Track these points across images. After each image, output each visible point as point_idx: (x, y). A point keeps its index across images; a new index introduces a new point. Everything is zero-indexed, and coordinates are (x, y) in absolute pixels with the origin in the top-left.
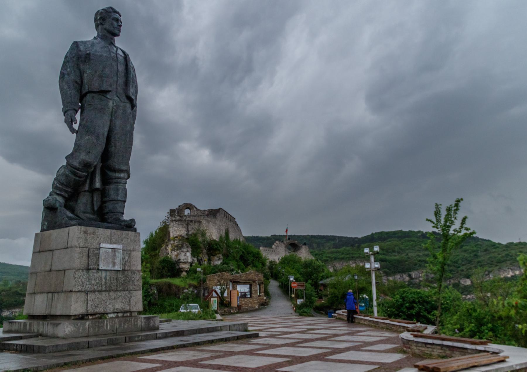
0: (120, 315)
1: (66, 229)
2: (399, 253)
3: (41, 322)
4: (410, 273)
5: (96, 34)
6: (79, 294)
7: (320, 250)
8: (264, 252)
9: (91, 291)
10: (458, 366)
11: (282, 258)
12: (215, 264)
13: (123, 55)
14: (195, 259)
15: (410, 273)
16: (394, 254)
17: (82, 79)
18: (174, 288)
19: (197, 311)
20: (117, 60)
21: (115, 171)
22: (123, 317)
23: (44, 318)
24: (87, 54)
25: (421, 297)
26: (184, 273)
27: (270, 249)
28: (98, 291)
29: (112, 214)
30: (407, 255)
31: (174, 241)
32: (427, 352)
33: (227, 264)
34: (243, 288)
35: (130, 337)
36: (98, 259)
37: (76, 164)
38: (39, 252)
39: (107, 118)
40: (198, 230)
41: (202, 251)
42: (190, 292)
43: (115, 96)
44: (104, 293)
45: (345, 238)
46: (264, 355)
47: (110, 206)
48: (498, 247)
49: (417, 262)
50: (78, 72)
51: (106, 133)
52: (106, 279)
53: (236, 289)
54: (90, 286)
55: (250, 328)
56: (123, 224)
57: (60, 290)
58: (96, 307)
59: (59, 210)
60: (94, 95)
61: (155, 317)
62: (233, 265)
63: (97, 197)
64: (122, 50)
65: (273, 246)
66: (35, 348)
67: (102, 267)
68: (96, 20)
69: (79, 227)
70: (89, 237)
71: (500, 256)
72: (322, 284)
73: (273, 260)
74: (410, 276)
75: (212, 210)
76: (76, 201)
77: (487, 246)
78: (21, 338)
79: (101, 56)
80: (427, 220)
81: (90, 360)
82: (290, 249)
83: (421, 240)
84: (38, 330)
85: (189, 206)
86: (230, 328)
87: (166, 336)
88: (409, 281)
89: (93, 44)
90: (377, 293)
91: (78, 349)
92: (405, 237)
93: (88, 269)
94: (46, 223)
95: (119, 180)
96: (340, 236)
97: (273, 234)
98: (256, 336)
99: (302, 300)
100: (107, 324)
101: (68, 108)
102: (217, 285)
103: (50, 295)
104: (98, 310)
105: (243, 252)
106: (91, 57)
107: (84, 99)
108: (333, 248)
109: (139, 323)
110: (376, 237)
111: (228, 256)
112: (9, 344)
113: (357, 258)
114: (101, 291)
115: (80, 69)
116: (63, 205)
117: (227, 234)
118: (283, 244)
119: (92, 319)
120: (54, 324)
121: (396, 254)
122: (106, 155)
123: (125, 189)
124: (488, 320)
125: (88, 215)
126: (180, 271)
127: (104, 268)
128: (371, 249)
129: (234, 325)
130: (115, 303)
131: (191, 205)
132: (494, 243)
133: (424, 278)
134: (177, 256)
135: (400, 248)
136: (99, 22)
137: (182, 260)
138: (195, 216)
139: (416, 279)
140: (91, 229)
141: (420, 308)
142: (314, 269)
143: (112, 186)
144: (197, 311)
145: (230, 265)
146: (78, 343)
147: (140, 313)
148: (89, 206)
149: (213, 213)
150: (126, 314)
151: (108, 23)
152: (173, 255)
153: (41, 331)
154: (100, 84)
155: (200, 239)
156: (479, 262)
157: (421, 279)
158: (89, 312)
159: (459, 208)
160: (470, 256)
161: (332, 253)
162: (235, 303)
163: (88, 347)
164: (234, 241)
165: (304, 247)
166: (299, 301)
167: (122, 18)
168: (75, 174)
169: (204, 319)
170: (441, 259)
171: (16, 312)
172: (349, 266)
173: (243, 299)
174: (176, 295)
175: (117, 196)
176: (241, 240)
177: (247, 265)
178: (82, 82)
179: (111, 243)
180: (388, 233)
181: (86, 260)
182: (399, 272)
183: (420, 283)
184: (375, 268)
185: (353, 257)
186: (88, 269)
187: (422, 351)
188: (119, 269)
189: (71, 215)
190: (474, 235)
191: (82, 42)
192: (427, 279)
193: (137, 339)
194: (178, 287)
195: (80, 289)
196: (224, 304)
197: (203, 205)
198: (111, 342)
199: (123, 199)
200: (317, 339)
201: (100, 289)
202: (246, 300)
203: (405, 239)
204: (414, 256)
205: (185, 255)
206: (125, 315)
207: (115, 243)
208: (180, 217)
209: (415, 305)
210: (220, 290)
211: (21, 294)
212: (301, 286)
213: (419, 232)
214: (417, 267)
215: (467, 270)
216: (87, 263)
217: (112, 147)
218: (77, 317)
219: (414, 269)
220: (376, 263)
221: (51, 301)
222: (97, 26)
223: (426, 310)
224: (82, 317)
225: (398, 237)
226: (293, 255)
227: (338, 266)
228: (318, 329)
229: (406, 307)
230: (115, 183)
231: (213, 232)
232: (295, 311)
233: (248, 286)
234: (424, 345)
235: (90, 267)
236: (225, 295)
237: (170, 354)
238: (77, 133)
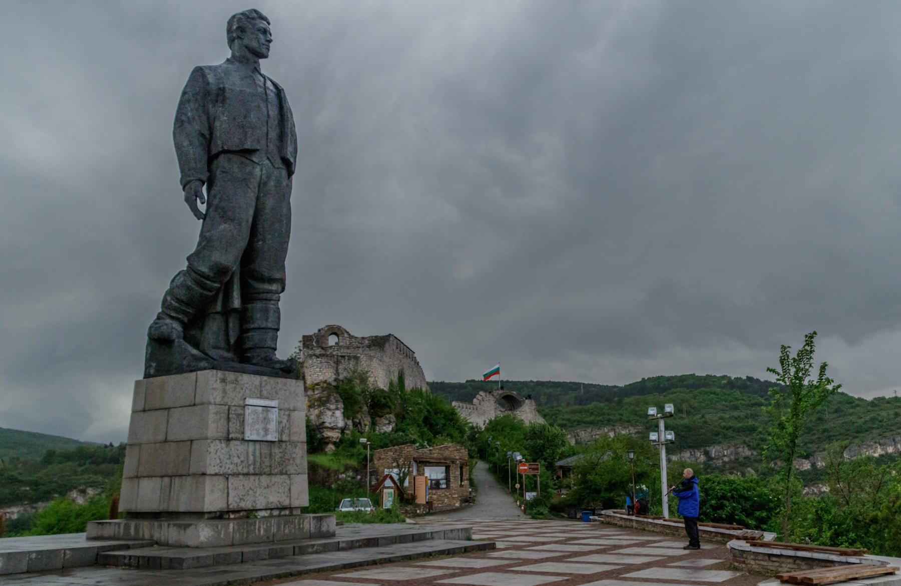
0: (276, 513)
1: (193, 375)
2: (688, 413)
3: (156, 524)
4: (707, 448)
5: (229, 54)
6: (215, 478)
7: (553, 407)
9: (234, 475)
10: (835, 577)
11: (491, 421)
12: (382, 431)
13: (274, 90)
14: (350, 423)
15: (707, 448)
16: (680, 415)
17: (211, 129)
18: (320, 471)
19: (369, 509)
20: (267, 99)
21: (263, 280)
22: (279, 516)
23: (155, 516)
24: (220, 89)
25: (736, 490)
26: (331, 447)
27: (468, 406)
28: (244, 474)
29: (258, 351)
30: (703, 416)
31: (313, 390)
32: (771, 568)
33: (404, 431)
34: (434, 473)
35: (300, 547)
36: (243, 423)
37: (204, 269)
38: (144, 411)
39: (252, 195)
40: (354, 372)
41: (361, 408)
42: (349, 479)
43: (265, 158)
44: (252, 478)
47: (255, 337)
48: (858, 406)
50: (204, 117)
51: (251, 219)
52: (254, 455)
53: (423, 474)
54: (232, 466)
55: (474, 537)
56: (278, 366)
57: (184, 473)
58: (241, 499)
59: (176, 344)
60: (231, 156)
61: (326, 517)
62: (413, 432)
63: (233, 323)
64: (271, 81)
65: (475, 400)
66: (163, 562)
67: (250, 435)
68: (229, 31)
69: (214, 371)
70: (228, 387)
71: (862, 420)
72: (561, 467)
73: (475, 425)
74: (707, 453)
75: (376, 337)
76: (202, 328)
77: (840, 402)
78: (128, 547)
80: (768, 369)
81: (319, 571)
82: (503, 407)
83: (728, 392)
84: (152, 536)
85: (336, 331)
86: (445, 535)
87: (352, 546)
88: (705, 463)
89: (227, 72)
91: (228, 565)
92: (699, 387)
93: (228, 440)
94: (154, 365)
95: (269, 296)
96: (586, 383)
97: (470, 379)
98: (492, 547)
99: (534, 494)
100: (259, 527)
101: (192, 178)
102: (393, 468)
103: (166, 480)
104: (243, 505)
105: (428, 411)
106: (227, 95)
107: (215, 162)
108: (575, 404)
109: (306, 526)
110: (323, 332)
111: (404, 418)
112: (115, 556)
113: (617, 421)
114: (247, 474)
115: (208, 113)
116: (182, 334)
117: (401, 378)
118: (491, 398)
119: (234, 519)
120: (179, 526)
121: (684, 415)
122: (249, 256)
123: (278, 311)
124: (849, 526)
125: (221, 352)
126: (324, 442)
127: (252, 438)
128: (661, 408)
129: (452, 531)
130: (266, 494)
131: (339, 328)
132: (852, 398)
133: (732, 457)
134: (319, 416)
135: (690, 406)
136: (234, 35)
137: (327, 425)
138: (348, 348)
139: (717, 459)
140: (231, 376)
141: (734, 508)
142: (548, 441)
143: (259, 305)
144: (369, 509)
145: (407, 432)
146: (227, 555)
147: (304, 510)
148: (222, 337)
149: (379, 343)
150: (285, 511)
153: (156, 536)
154: (240, 139)
155: (358, 389)
156: (825, 431)
157: (726, 459)
158: (231, 507)
159: (814, 348)
160: (811, 421)
161: (574, 412)
162: (422, 497)
163: (242, 562)
164: (412, 391)
165: (527, 401)
166: (529, 496)
167: (272, 28)
168: (203, 287)
169: (389, 522)
170: (790, 429)
171: (13, 513)
172: (606, 436)
173: (434, 492)
174: (323, 484)
175: (267, 320)
176: (424, 389)
177: (436, 433)
178: (211, 134)
179: (261, 397)
180: (669, 379)
181: (225, 423)
182: (689, 447)
183: (724, 466)
184: (667, 440)
185: (609, 420)
186: (228, 440)
187: (763, 567)
188: (274, 440)
189: (195, 352)
190: (839, 390)
191: (210, 68)
192: (737, 459)
193: (310, 550)
194: (327, 470)
195: (217, 471)
196: (405, 498)
197: (361, 330)
198: (274, 555)
199: (276, 327)
201: (245, 471)
202: (439, 492)
203: (698, 390)
204: (715, 418)
205: (332, 416)
206: (283, 513)
207: (267, 398)
208: (323, 348)
209: (727, 503)
210: (399, 474)
211: (22, 481)
212: (534, 469)
213: (724, 377)
214: (719, 438)
215: (806, 444)
216: (226, 428)
217: (258, 241)
218: (213, 515)
219: (714, 443)
220: (668, 432)
221: (168, 490)
222: (231, 41)
223: (744, 510)
224: (220, 516)
225: (687, 387)
226: (508, 416)
227: (584, 435)
228: (584, 538)
229: (711, 506)
230: (266, 300)
231: (379, 376)
232: (525, 512)
233: (444, 468)
234: (767, 558)
235: (230, 436)
236: (406, 484)
237: (386, 570)
238: (204, 219)
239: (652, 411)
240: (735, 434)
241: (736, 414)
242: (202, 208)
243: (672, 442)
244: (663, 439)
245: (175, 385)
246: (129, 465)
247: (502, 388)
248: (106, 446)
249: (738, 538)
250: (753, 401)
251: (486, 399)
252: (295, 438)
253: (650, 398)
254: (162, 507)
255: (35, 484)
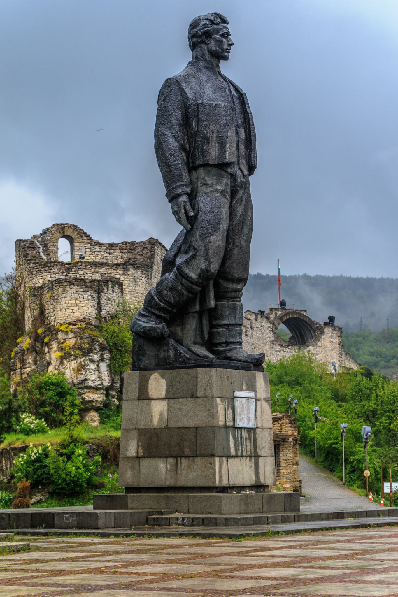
79: (217, 106)
151: (209, 40)
152: (69, 372)
251: (256, 324)
252: (265, 425)
254: (170, 482)
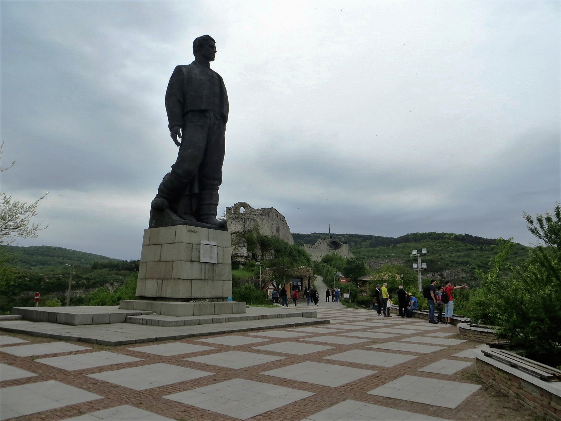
8: (307, 249)
45: (381, 237)
46: (310, 342)
49: (449, 262)
65: (316, 244)
67: (203, 260)
74: (441, 275)
81: (239, 331)
82: (331, 247)
85: (244, 205)
90: (40, 312)
93: (192, 261)
98: (328, 322)
103: (160, 281)
108: (370, 247)
110: (237, 206)
128: (419, 251)
131: (245, 203)
140: (192, 228)
155: (255, 236)
161: (369, 251)
165: (345, 245)
171: (77, 293)
174: (393, 283)
200: (359, 330)
203: (438, 241)
220: (423, 264)
239: (414, 252)
240: (457, 265)
241: (458, 254)
242: (180, 140)
243: (425, 269)
244: (420, 267)
245: (166, 232)
246: (141, 273)
247: (331, 237)
248: (123, 261)
249: (463, 322)
250: (468, 247)
253: (411, 244)
255: (88, 279)
